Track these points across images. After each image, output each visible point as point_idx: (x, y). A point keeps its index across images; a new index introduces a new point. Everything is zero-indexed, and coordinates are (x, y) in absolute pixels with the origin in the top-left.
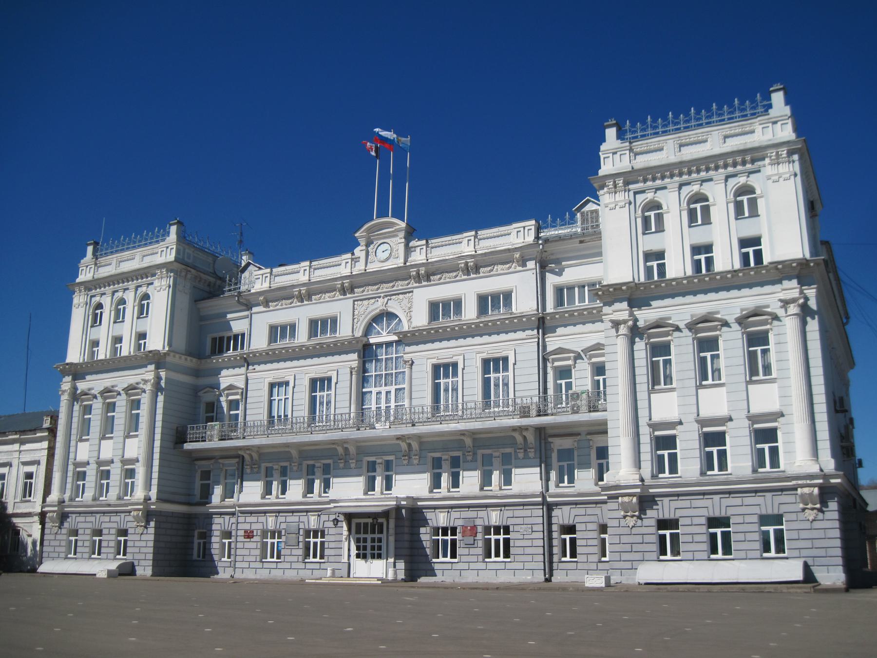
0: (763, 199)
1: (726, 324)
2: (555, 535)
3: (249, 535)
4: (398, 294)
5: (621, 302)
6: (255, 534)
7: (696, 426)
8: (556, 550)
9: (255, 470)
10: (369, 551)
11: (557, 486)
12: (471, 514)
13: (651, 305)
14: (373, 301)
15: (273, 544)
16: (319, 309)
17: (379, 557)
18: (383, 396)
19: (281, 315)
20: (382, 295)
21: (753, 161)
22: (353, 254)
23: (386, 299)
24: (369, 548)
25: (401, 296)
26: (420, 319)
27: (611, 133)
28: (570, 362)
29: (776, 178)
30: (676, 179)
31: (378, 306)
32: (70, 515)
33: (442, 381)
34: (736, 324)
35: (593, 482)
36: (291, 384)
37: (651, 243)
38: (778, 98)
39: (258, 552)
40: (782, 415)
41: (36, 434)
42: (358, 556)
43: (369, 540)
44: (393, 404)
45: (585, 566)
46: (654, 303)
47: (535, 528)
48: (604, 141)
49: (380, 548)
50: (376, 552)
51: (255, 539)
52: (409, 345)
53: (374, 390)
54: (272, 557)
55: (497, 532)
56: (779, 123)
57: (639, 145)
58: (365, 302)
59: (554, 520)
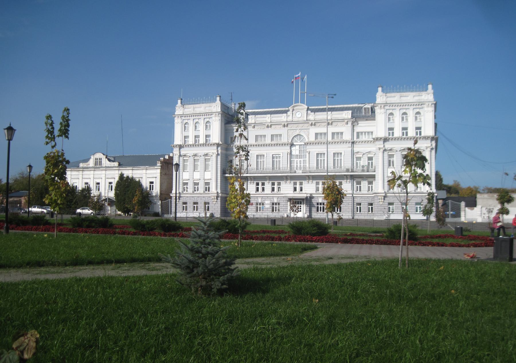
2: (355, 206)
6: (253, 204)
8: (355, 210)
11: (356, 192)
14: (295, 131)
15: (260, 207)
18: (299, 162)
22: (287, 114)
23: (300, 131)
25: (305, 130)
26: (312, 139)
27: (380, 89)
28: (361, 156)
30: (193, 117)
31: (297, 132)
35: (367, 191)
36: (265, 156)
37: (186, 134)
38: (430, 87)
39: (255, 210)
44: (302, 165)
45: (364, 215)
47: (350, 204)
48: (177, 104)
50: (299, 210)
53: (295, 160)
55: (260, 204)
56: (430, 95)
57: (388, 95)
58: (292, 131)
59: (355, 202)
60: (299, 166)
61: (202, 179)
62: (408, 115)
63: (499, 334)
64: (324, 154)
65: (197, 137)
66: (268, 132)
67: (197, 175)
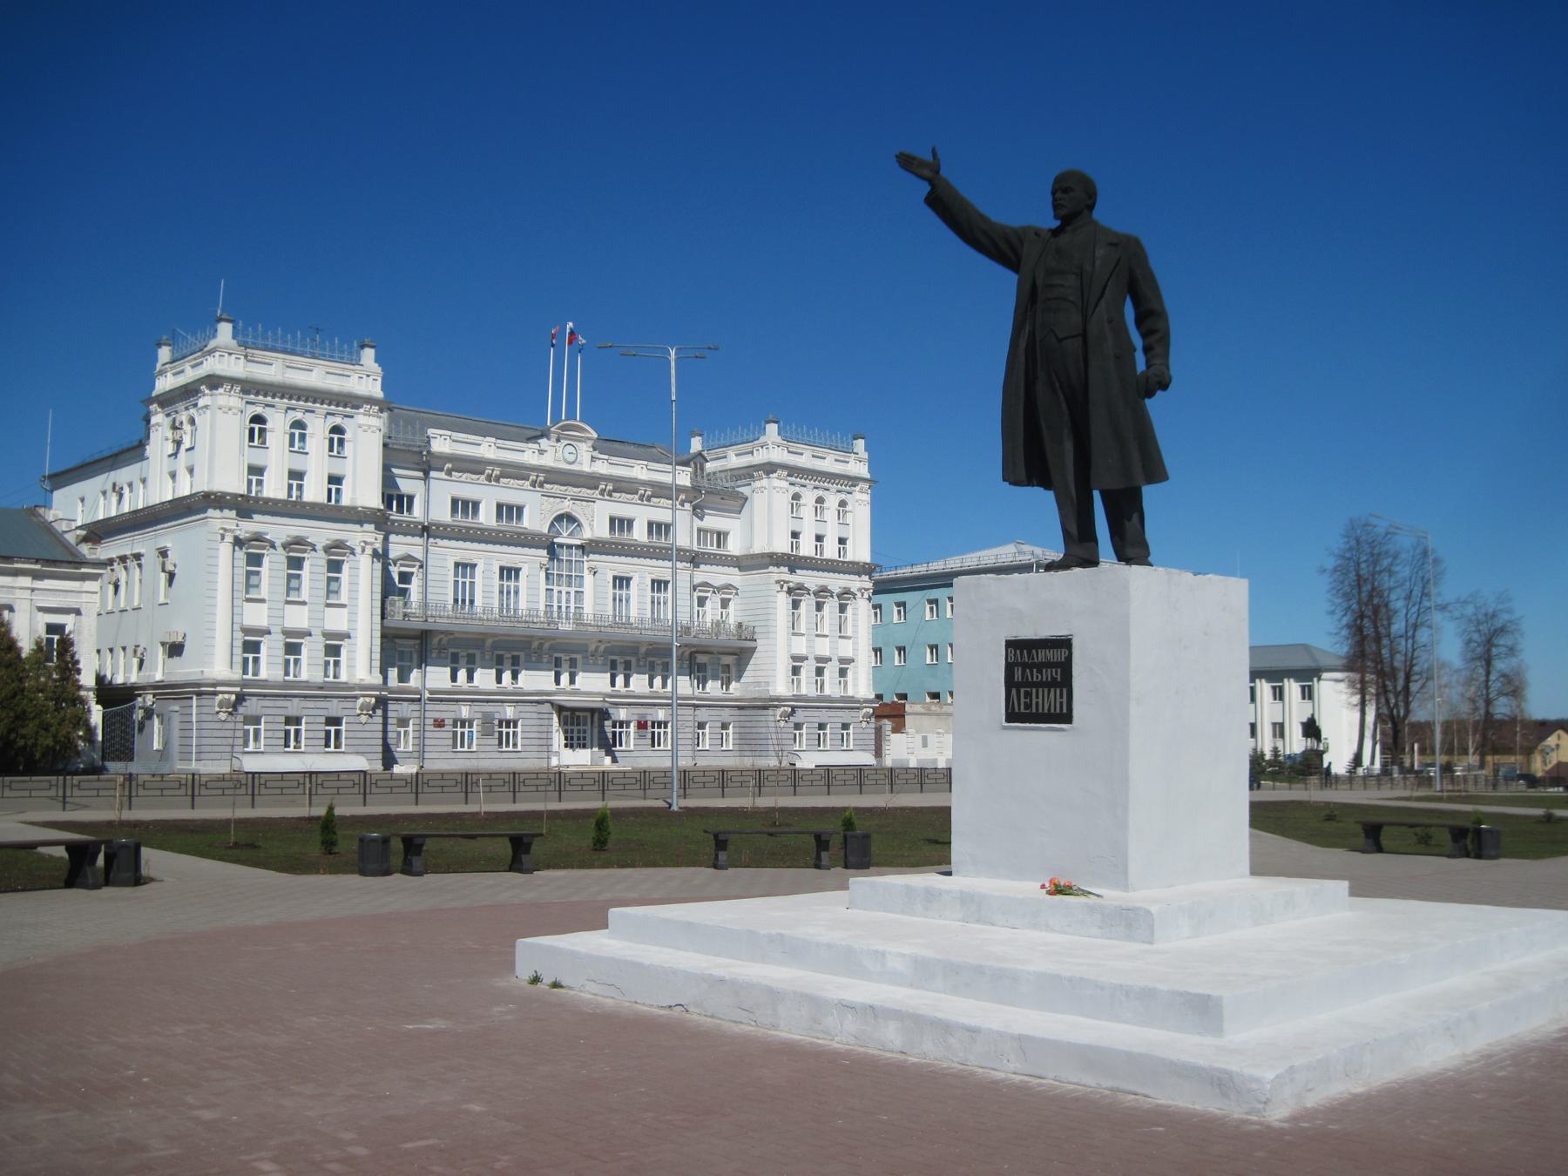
0: (352, 443)
1: (273, 546)
3: (439, 724)
4: (582, 500)
5: (231, 510)
6: (446, 722)
7: (282, 637)
9: (443, 655)
10: (575, 741)
12: (642, 710)
13: (252, 518)
14: (558, 500)
16: (511, 493)
17: (584, 746)
19: (467, 488)
20: (569, 498)
21: (852, 486)
24: (575, 739)
29: (226, 410)
32: (246, 697)
33: (460, 580)
34: (323, 552)
37: (257, 458)
40: (349, 637)
41: (80, 569)
42: (566, 746)
43: (575, 732)
44: (572, 605)
46: (256, 517)
49: (584, 738)
50: (582, 742)
51: (446, 728)
52: (442, 538)
54: (462, 746)
56: (234, 356)
60: (564, 609)
61: (316, 632)
62: (268, 426)
63: (876, 1016)
64: (666, 583)
65: (296, 475)
66: (489, 497)
67: (297, 618)
